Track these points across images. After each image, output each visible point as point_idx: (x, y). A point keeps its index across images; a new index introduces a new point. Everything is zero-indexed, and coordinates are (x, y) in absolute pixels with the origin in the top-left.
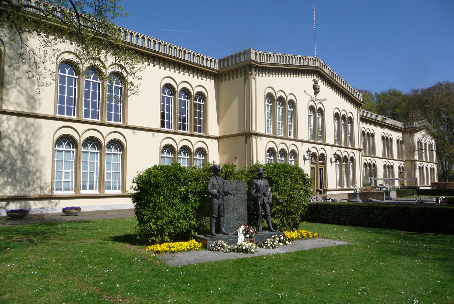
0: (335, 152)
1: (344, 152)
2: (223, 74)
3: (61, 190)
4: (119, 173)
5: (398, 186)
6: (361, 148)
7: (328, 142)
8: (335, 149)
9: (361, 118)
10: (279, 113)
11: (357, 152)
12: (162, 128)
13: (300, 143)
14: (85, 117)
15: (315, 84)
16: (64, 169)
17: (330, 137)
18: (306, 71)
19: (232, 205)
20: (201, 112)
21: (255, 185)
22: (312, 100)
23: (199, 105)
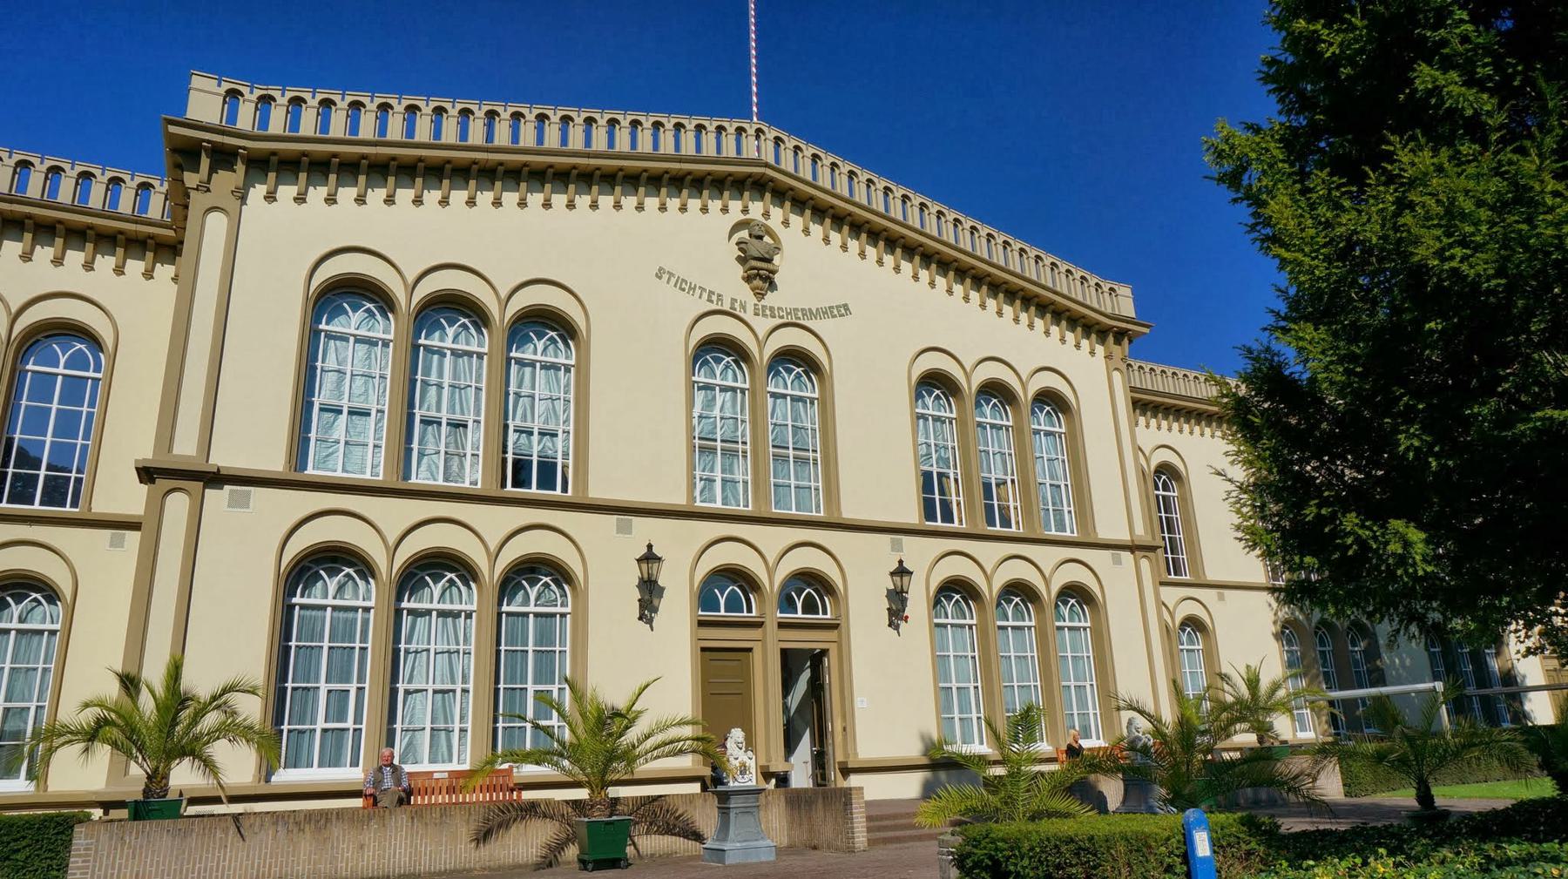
4: (973, 657)
5: (1377, 628)
7: (1104, 533)
16: (535, 682)
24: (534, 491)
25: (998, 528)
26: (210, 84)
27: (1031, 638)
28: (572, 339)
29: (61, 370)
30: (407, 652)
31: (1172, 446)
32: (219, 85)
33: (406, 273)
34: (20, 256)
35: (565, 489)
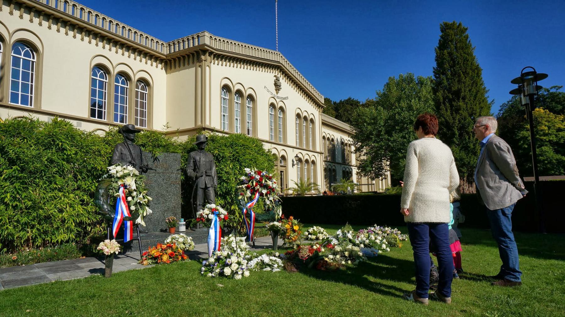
0: (297, 155)
1: (305, 155)
2: (172, 60)
6: (323, 151)
7: (289, 143)
8: (297, 151)
9: (322, 122)
10: (236, 108)
11: (318, 156)
15: (276, 81)
17: (292, 139)
18: (267, 65)
19: (156, 189)
20: (143, 102)
21: (192, 160)
22: (273, 97)
23: (142, 94)
25: (139, 126)
29: (22, 57)
31: (147, 71)
34: (19, 17)
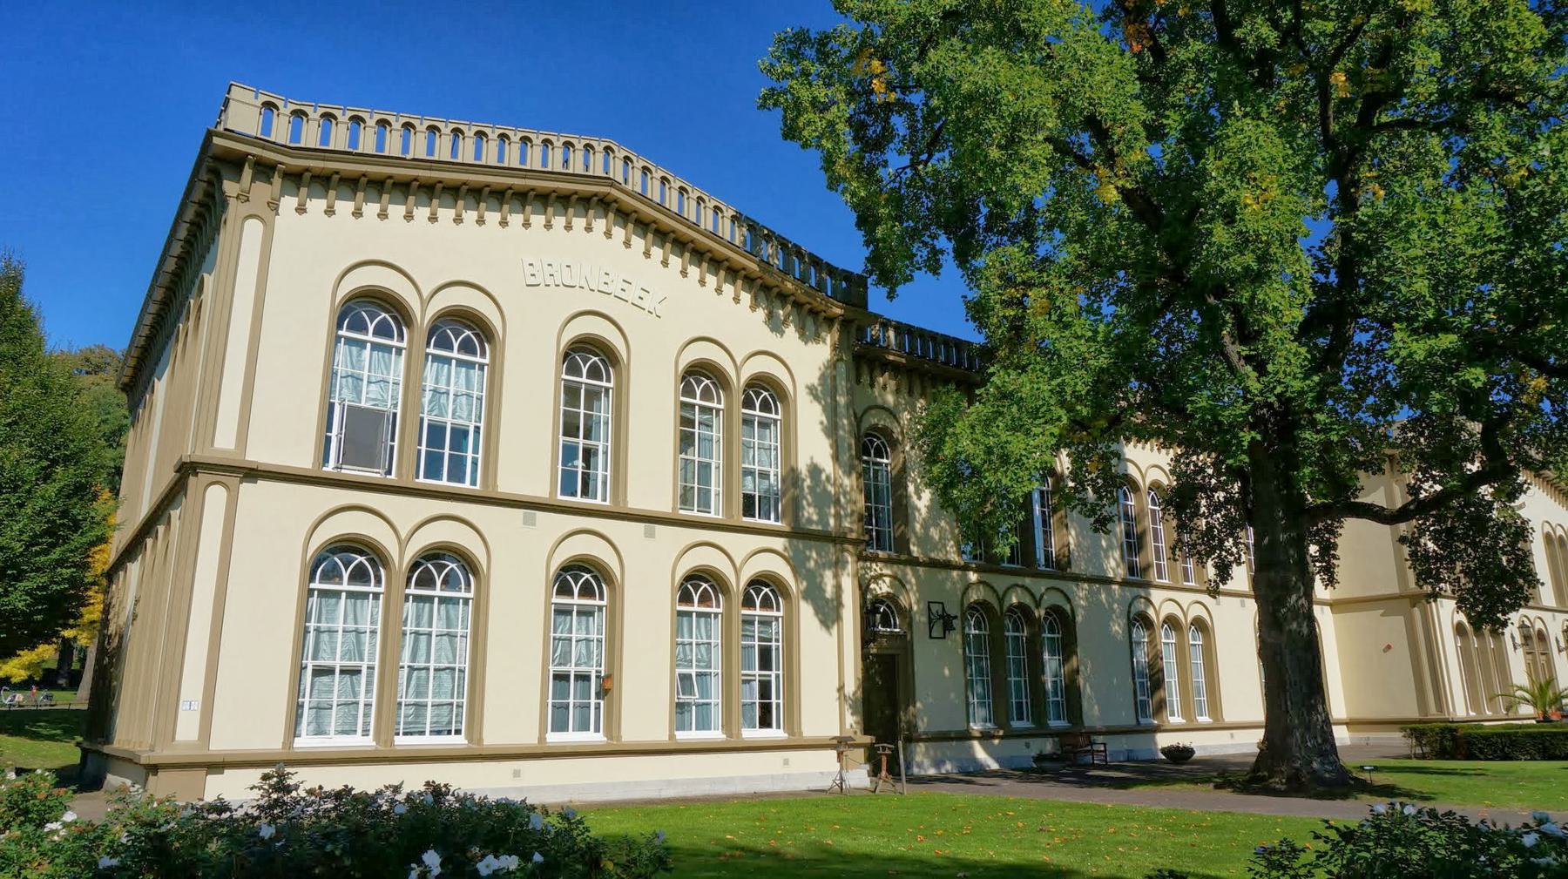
3: (422, 733)
12: (745, 519)
13: (1550, 614)
14: (563, 493)
24: (444, 483)
26: (248, 96)
27: (717, 626)
28: (489, 342)
30: (318, 630)
32: (256, 98)
33: (423, 291)
35: (473, 482)
